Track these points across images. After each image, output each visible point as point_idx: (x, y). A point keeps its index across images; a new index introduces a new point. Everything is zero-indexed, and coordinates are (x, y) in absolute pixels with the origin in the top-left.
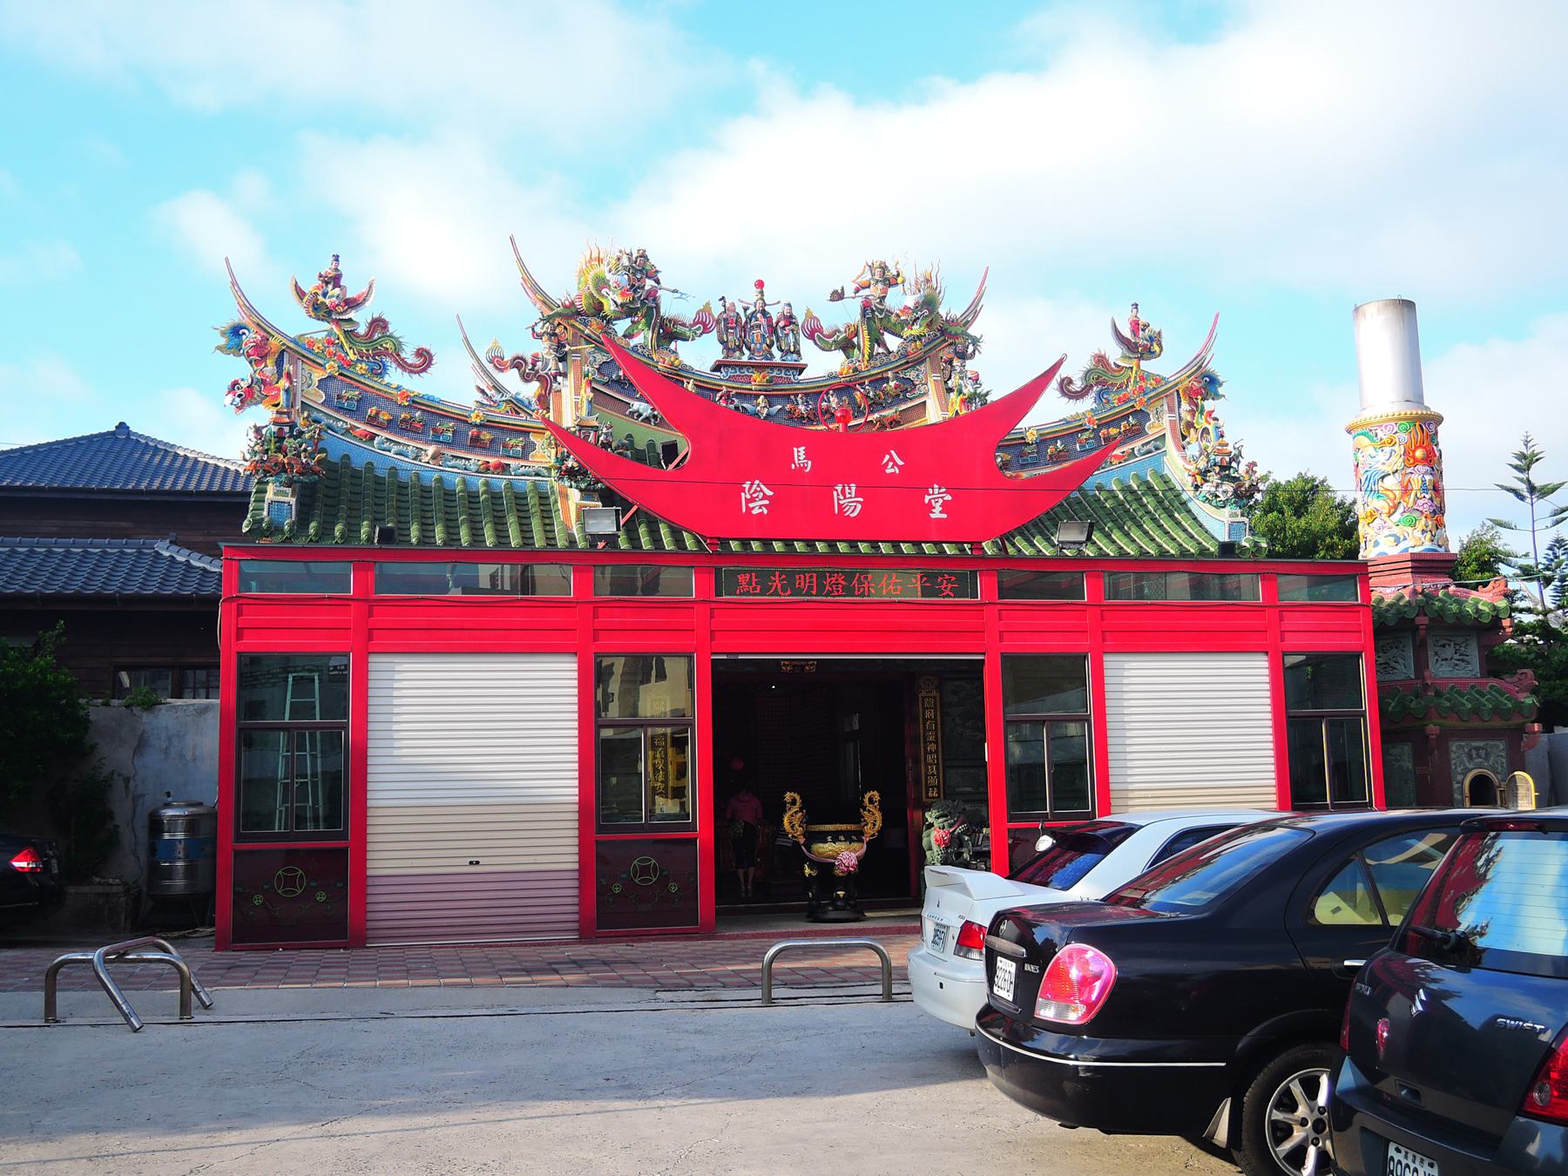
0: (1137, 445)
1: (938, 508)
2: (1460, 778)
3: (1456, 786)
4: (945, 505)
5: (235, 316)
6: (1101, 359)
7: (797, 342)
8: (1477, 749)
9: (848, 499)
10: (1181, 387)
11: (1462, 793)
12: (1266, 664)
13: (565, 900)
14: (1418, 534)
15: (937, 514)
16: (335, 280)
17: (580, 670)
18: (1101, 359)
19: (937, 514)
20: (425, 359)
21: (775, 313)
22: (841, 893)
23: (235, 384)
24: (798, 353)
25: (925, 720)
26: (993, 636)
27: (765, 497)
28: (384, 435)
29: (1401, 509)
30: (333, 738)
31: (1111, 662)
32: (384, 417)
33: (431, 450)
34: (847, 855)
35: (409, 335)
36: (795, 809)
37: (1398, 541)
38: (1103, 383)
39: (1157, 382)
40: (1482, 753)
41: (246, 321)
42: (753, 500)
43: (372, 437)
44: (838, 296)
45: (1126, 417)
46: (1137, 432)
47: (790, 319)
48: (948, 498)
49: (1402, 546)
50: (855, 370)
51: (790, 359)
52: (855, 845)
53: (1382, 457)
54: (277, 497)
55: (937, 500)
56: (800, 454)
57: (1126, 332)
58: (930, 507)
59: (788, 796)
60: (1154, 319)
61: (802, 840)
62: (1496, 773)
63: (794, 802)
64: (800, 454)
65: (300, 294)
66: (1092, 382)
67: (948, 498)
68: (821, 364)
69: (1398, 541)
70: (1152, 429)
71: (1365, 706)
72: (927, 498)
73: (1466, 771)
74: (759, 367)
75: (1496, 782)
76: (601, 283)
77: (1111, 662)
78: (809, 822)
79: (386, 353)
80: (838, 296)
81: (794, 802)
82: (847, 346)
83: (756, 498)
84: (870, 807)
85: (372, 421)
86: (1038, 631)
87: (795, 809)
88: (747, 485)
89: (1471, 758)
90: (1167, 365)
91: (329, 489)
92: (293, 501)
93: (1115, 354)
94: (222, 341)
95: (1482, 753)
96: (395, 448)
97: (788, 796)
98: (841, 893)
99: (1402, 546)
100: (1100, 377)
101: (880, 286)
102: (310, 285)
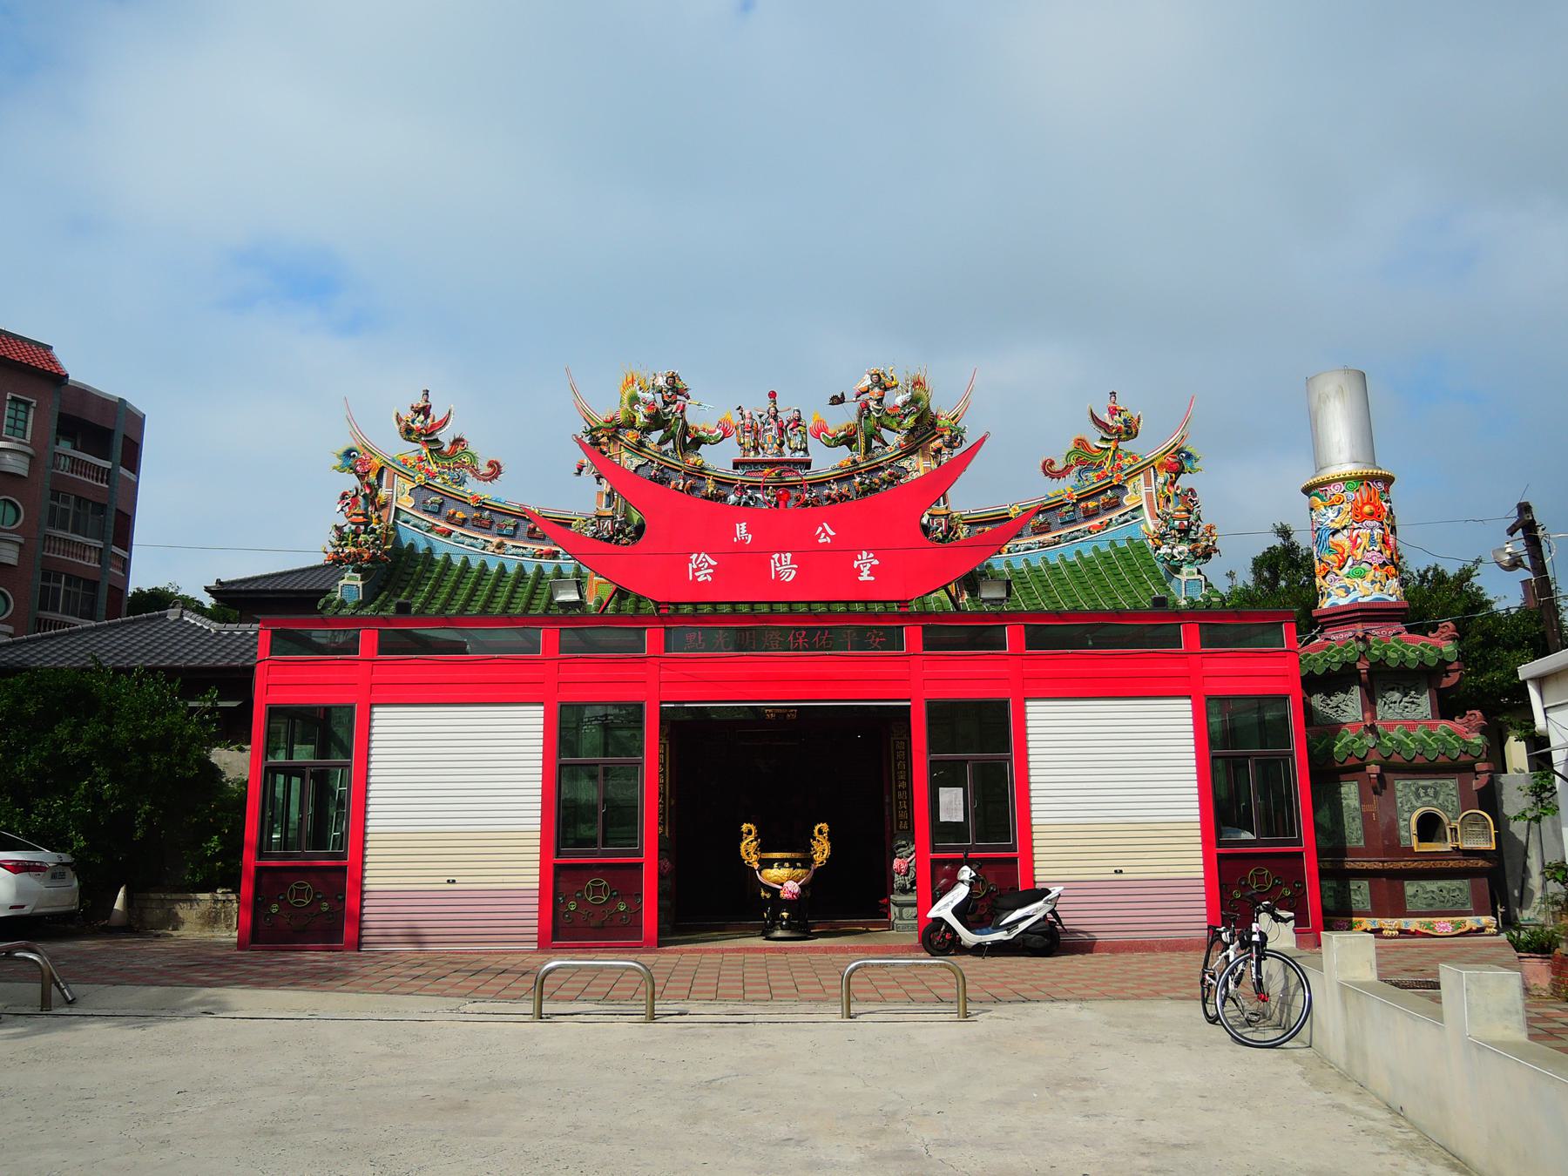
0: (1115, 515)
1: (866, 572)
2: (1406, 815)
3: (1402, 823)
4: (873, 570)
5: (349, 443)
6: (1081, 443)
7: (804, 441)
8: (1425, 788)
9: (784, 567)
10: (1156, 464)
11: (1409, 831)
12: (1190, 707)
13: (529, 915)
14: (1366, 584)
15: (865, 576)
16: (425, 411)
17: (1194, 711)
18: (1081, 443)
19: (865, 576)
20: (496, 469)
21: (784, 417)
22: (785, 914)
23: (344, 496)
24: (805, 450)
25: (897, 761)
26: (914, 682)
27: (710, 566)
28: (458, 530)
29: (1350, 562)
30: (321, 780)
31: (379, 713)
32: (460, 515)
33: (496, 540)
34: (784, 879)
35: (482, 449)
36: (751, 838)
37: (1348, 592)
38: (1082, 463)
39: (1135, 459)
40: (1431, 792)
41: (355, 445)
42: (699, 569)
43: (450, 533)
44: (838, 400)
45: (1105, 491)
46: (1115, 505)
47: (797, 421)
48: (876, 562)
49: (1352, 596)
50: (854, 462)
51: (799, 455)
52: (799, 871)
53: (1331, 514)
54: (350, 584)
55: (865, 563)
56: (741, 529)
57: (1105, 417)
58: (859, 571)
59: (745, 827)
60: (1132, 407)
61: (756, 866)
62: (1445, 809)
63: (750, 832)
64: (741, 529)
65: (399, 420)
66: (1073, 462)
67: (876, 562)
68: (826, 460)
69: (1348, 592)
70: (1128, 501)
71: (1294, 748)
72: (856, 564)
73: (1413, 809)
74: (771, 464)
75: (1446, 820)
76: (634, 400)
77: (379, 713)
78: (762, 851)
79: (463, 465)
80: (838, 400)
81: (750, 832)
82: (848, 441)
83: (702, 567)
84: (819, 837)
85: (450, 519)
86: (965, 677)
87: (751, 838)
88: (694, 557)
89: (1418, 796)
90: (1149, 446)
91: (393, 569)
92: (360, 584)
93: (1094, 438)
94: (338, 462)
95: (1431, 792)
96: (468, 541)
97: (745, 827)
98: (785, 914)
99: (1352, 596)
100: (1083, 457)
101: (877, 390)
102: (407, 414)
